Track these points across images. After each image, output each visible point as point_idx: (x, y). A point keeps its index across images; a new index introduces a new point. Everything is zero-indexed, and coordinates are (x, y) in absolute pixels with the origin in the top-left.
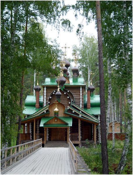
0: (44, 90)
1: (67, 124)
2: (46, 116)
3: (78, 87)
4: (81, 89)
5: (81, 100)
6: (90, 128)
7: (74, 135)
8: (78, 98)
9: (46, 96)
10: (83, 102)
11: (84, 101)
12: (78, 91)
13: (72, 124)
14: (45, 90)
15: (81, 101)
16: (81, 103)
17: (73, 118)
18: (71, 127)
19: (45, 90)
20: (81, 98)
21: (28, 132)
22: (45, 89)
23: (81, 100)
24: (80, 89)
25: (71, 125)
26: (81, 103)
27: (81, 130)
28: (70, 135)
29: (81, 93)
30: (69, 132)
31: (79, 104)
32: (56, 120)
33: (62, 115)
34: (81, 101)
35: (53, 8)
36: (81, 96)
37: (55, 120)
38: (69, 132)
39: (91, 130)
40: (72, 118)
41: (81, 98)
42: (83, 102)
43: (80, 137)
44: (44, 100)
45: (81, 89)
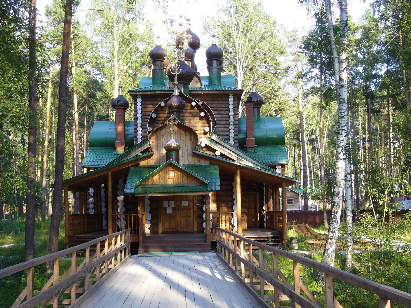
0: (136, 105)
3: (191, 249)
4: (231, 100)
5: (232, 127)
6: (258, 197)
8: (225, 122)
9: (142, 119)
10: (237, 126)
11: (240, 131)
12: (224, 106)
13: (219, 184)
14: (139, 104)
15: (232, 131)
16: (232, 135)
17: (219, 167)
19: (139, 104)
20: (232, 123)
21: (98, 210)
22: (139, 100)
23: (232, 127)
24: (230, 100)
26: (232, 135)
27: (242, 185)
29: (231, 110)
31: (227, 133)
34: (232, 131)
35: (44, 79)
36: (231, 117)
39: (260, 199)
40: (217, 167)
41: (232, 123)
42: (237, 126)
44: (136, 129)
45: (231, 100)
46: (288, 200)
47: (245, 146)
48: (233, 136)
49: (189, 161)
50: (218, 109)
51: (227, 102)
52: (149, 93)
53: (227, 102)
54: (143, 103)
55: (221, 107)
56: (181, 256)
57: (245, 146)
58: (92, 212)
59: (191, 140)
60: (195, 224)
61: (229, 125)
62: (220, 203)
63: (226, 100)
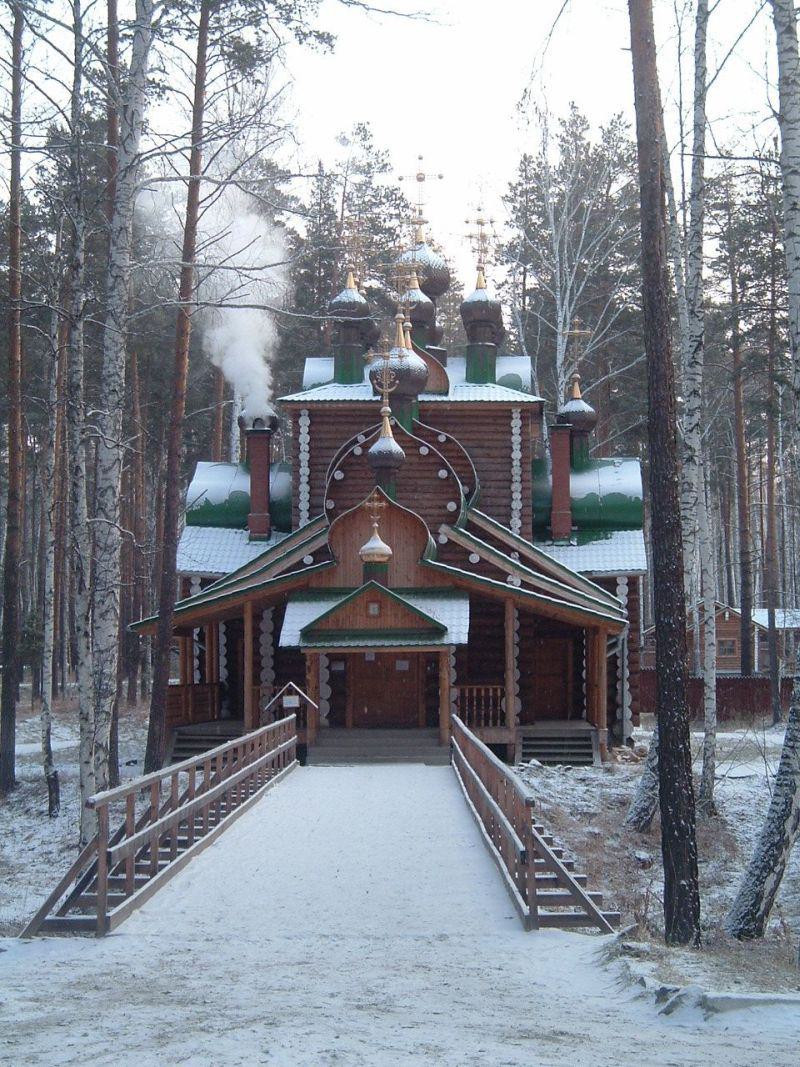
1: (440, 631)
2: (314, 584)
7: (479, 691)
8: (501, 476)
9: (311, 465)
16: (517, 505)
18: (459, 647)
24: (513, 424)
25: (464, 639)
26: (517, 505)
28: (455, 692)
30: (448, 675)
32: (374, 609)
33: (412, 576)
36: (516, 463)
37: (367, 607)
38: (448, 675)
43: (513, 705)
46: (732, 651)
47: (549, 528)
48: (519, 508)
49: (409, 580)
50: (486, 444)
51: (506, 429)
52: (341, 405)
53: (506, 429)
54: (313, 428)
55: (492, 440)
56: (480, 829)
57: (549, 528)
58: (196, 682)
59: (415, 537)
60: (422, 707)
61: (511, 482)
62: (642, 446)
63: (503, 425)
